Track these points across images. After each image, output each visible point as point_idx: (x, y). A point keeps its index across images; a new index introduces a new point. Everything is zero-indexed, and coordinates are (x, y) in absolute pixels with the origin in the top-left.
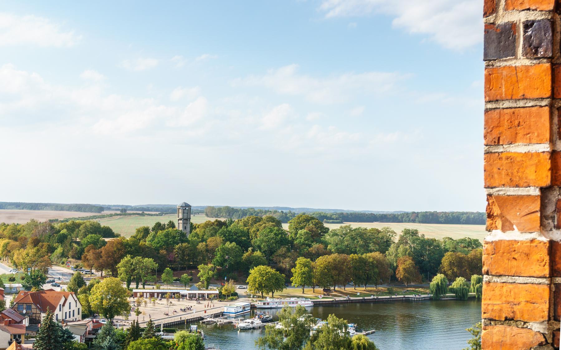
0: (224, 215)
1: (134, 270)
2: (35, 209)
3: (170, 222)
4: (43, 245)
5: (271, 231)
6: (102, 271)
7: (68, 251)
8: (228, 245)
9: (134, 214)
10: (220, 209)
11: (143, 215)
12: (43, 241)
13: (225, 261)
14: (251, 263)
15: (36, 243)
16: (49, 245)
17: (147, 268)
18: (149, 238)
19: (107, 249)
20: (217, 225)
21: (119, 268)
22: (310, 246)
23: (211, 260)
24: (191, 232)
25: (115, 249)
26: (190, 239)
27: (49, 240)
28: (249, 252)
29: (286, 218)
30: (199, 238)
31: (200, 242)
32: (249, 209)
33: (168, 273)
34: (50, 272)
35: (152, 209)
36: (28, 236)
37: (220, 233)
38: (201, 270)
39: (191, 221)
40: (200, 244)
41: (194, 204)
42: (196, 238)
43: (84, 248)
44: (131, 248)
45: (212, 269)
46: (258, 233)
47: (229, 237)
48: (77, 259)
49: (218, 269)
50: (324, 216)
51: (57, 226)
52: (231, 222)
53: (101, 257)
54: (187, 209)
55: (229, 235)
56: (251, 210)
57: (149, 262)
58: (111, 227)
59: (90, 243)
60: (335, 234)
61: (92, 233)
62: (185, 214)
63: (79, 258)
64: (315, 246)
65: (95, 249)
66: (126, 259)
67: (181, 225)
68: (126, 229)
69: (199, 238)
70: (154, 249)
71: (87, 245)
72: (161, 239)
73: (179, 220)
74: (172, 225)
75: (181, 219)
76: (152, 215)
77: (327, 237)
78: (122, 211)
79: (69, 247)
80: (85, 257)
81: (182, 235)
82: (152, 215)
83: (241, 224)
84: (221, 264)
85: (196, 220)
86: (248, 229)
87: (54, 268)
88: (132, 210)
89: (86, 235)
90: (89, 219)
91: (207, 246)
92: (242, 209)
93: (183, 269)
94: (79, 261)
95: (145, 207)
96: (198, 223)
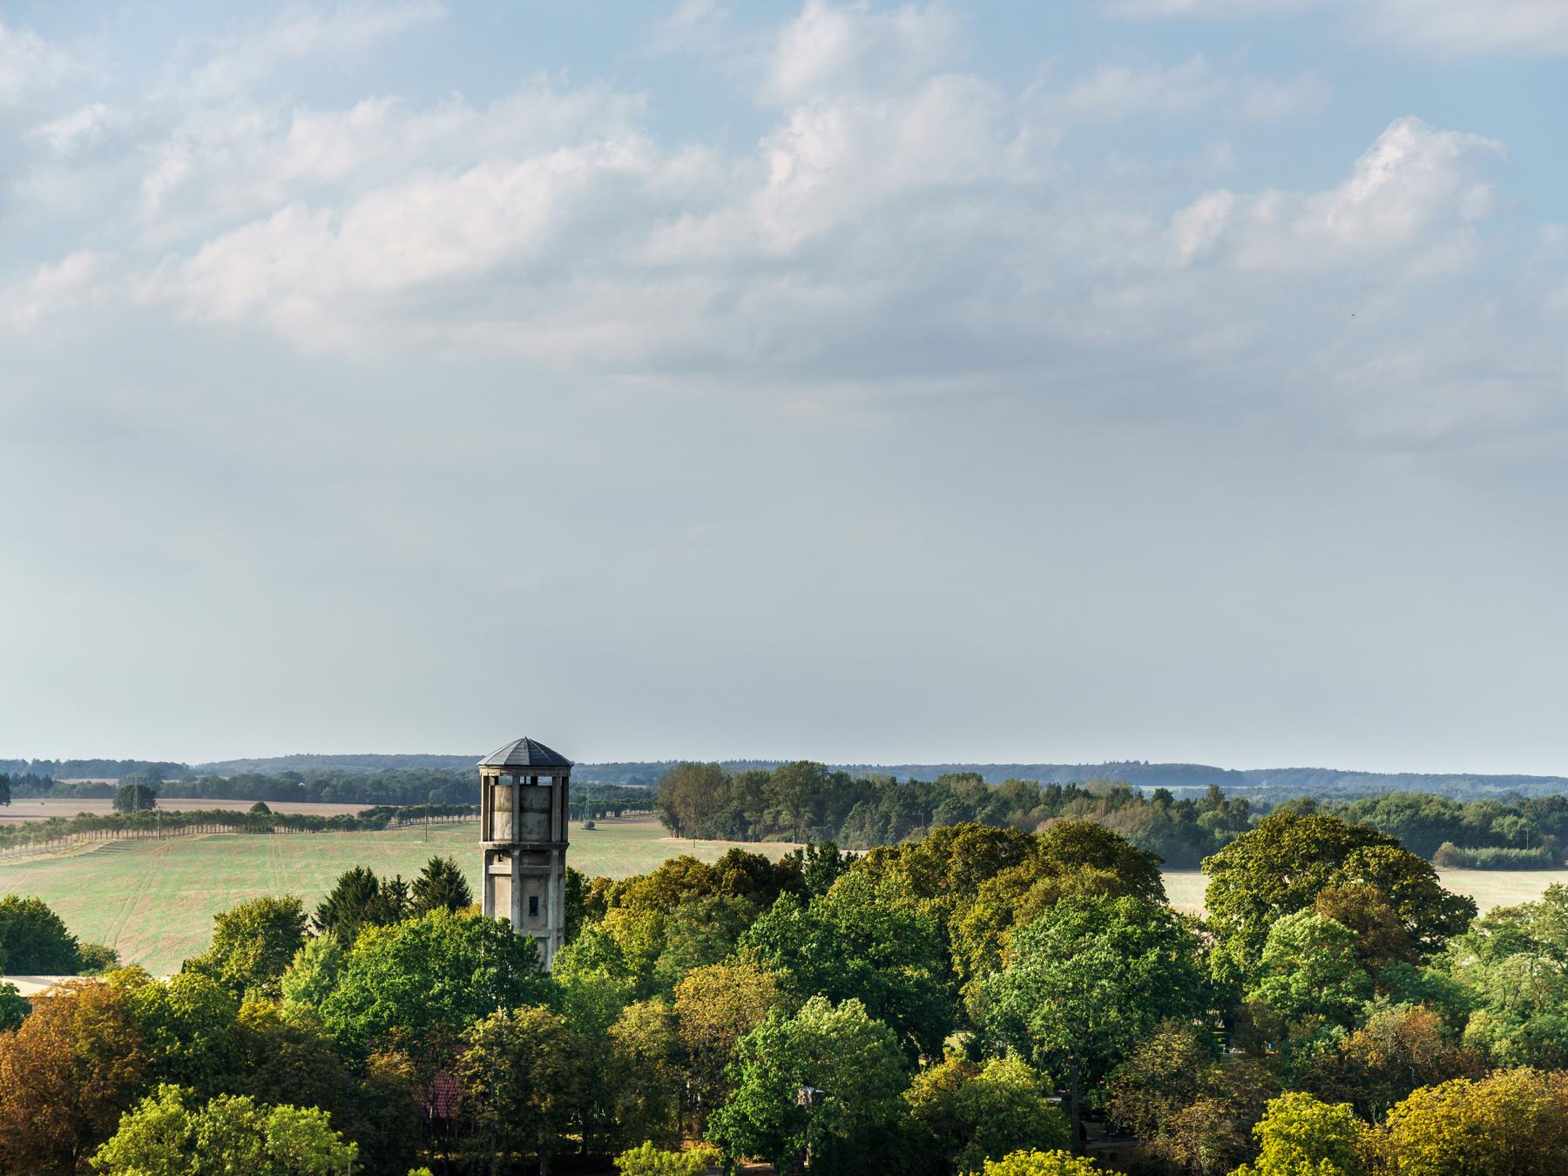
0: (786, 818)
3: (437, 868)
5: (1096, 922)
8: (817, 1015)
11: (259, 823)
13: (795, 1119)
18: (299, 975)
20: (739, 887)
22: (1349, 1018)
24: (569, 932)
25: (83, 1047)
26: (563, 980)
28: (951, 1063)
29: (1195, 822)
37: (762, 937)
39: (574, 861)
40: (633, 1012)
41: (588, 751)
44: (186, 1039)
46: (1007, 936)
52: (832, 866)
54: (543, 791)
56: (961, 788)
58: (55, 910)
60: (1512, 940)
62: (532, 819)
64: (1387, 1017)
66: (151, 1111)
67: (505, 889)
70: (335, 1046)
72: (380, 977)
74: (445, 886)
76: (316, 825)
77: (1463, 962)
81: (515, 953)
82: (316, 825)
83: (896, 876)
85: (605, 854)
86: (943, 913)
88: (193, 794)
91: (673, 1021)
95: (270, 772)
96: (618, 877)
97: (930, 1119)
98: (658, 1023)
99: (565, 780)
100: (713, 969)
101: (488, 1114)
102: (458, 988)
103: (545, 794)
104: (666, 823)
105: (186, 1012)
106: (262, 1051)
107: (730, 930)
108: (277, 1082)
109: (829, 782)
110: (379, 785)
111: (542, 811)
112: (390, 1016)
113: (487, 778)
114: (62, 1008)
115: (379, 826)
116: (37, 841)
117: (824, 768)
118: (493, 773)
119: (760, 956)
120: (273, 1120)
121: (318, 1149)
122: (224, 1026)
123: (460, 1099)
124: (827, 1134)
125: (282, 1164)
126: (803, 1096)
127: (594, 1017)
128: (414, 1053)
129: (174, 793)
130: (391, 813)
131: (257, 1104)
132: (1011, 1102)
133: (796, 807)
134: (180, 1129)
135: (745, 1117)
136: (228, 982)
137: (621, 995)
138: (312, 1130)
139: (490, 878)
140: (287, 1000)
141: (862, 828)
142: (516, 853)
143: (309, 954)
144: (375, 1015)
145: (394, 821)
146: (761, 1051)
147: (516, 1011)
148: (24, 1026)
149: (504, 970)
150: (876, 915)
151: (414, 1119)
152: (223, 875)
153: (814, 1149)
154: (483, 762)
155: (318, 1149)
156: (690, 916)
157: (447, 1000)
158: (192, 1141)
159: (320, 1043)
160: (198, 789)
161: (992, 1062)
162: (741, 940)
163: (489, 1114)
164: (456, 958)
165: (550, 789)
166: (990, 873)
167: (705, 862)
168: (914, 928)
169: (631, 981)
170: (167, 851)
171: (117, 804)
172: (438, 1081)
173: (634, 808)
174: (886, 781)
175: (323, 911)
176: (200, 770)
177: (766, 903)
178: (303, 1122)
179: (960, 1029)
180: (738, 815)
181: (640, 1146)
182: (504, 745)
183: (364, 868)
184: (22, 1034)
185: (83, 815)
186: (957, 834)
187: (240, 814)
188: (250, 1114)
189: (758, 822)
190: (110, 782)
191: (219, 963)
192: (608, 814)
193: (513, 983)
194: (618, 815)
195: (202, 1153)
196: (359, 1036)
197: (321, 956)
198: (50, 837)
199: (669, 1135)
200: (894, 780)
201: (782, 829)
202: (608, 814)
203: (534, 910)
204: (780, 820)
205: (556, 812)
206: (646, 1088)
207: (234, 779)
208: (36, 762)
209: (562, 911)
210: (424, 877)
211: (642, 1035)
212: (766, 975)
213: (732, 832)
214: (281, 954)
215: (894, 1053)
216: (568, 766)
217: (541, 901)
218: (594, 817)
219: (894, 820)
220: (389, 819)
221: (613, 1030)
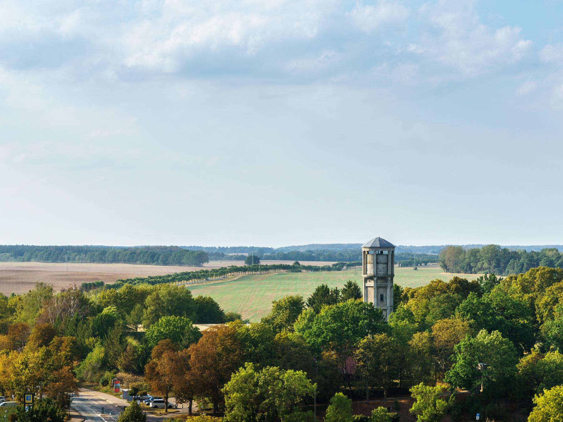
0: (486, 265)
1: (261, 397)
2: (55, 261)
3: (350, 284)
4: (61, 342)
6: (191, 400)
7: (117, 355)
8: (483, 336)
9: (275, 267)
10: (475, 253)
11: (296, 269)
12: (63, 333)
13: (477, 375)
14: (539, 380)
15: (47, 336)
16: (74, 342)
17: (291, 392)
18: (299, 324)
19: (201, 349)
20: (457, 290)
21: (227, 393)
23: (441, 372)
24: (394, 308)
25: (219, 349)
26: (392, 324)
27: (75, 331)
28: (534, 354)
30: (413, 321)
31: (415, 331)
32: (545, 250)
33: (340, 404)
34: (75, 402)
35: (320, 255)
36: (29, 321)
37: (464, 309)
38: (419, 397)
40: (417, 336)
41: (401, 240)
42: (406, 321)
43: (151, 348)
44: (256, 346)
45: (443, 395)
46: (555, 308)
47: (483, 319)
48: (135, 373)
49: (458, 396)
50: (87, 250)
51: (94, 297)
52: (493, 282)
53: (189, 369)
55: (483, 314)
56: (550, 254)
57: (293, 377)
58: (216, 300)
59: (165, 336)
61: (170, 313)
62: (381, 266)
63: (140, 372)
65: (174, 350)
66: (243, 372)
67: (372, 293)
68: (250, 304)
69: (413, 322)
70: (309, 348)
71: (158, 339)
72: (326, 324)
73: (366, 280)
74: (353, 291)
75: (371, 278)
76: (316, 269)
78: (249, 260)
79: (118, 347)
80: (153, 369)
81: (375, 315)
82: (316, 269)
83: (515, 286)
84: (468, 383)
85: (405, 278)
86: (533, 299)
87: (85, 394)
88: (274, 258)
89: (158, 317)
90: (173, 280)
91: (432, 339)
92: (528, 251)
93: (377, 395)
94: (141, 378)
95: (302, 250)
96: (414, 287)
97: (526, 375)
98: (426, 340)
99: (393, 252)
100: (446, 320)
101: (365, 373)
102: (354, 328)
103: (385, 257)
104: (442, 267)
105: (256, 337)
106: (283, 350)
107: (453, 306)
108: (289, 361)
109: (501, 252)
110: (341, 255)
111: (384, 264)
112: (330, 338)
113: (364, 252)
114: (212, 335)
115: (339, 269)
116: (216, 276)
117: (499, 247)
118: (367, 250)
119: (463, 316)
120: (286, 375)
121: (302, 386)
122: (269, 342)
123: (355, 367)
124: (488, 380)
125: (290, 391)
126: (480, 366)
127: (403, 337)
128: (338, 350)
129: (268, 258)
130: (344, 264)
131: (280, 369)
132: (556, 368)
133: (490, 261)
134: (253, 379)
135: (458, 374)
136: (276, 326)
137: (413, 330)
138: (300, 379)
139: (366, 288)
140: (295, 332)
141: (514, 268)
142: (375, 279)
143: (303, 315)
144: (324, 338)
145: (345, 267)
146: (463, 349)
147: (375, 336)
148: (199, 342)
149: (371, 321)
150: (506, 300)
151: (338, 375)
152: (282, 287)
153: (484, 385)
154: (363, 246)
155: (302, 386)
156: (437, 301)
157: (350, 332)
158: (257, 382)
159: (304, 348)
160: (276, 257)
161: (548, 354)
162: (456, 310)
163: (365, 373)
164: (353, 317)
165: (387, 255)
166: (550, 285)
167: (445, 281)
168: (521, 305)
169: (416, 325)
170: (262, 279)
171: (246, 263)
172: (347, 361)
173: (432, 262)
174: (522, 251)
175: (310, 300)
176: (278, 250)
177: (465, 296)
178: (297, 376)
179: (539, 342)
180: (469, 264)
181: (419, 384)
182: (371, 239)
183: (325, 285)
184: (199, 345)
185: (232, 266)
186: (538, 271)
187: (289, 266)
188: (278, 373)
189: (475, 267)
190: (245, 254)
191: (273, 319)
192: (423, 264)
193: (374, 326)
194: (426, 264)
195: (261, 387)
196: (318, 346)
197: (308, 316)
198: (221, 274)
199: (430, 380)
200: (525, 251)
201: (484, 269)
202: (423, 264)
203: (382, 299)
204: (484, 266)
205: (390, 264)
206: (422, 363)
207: (289, 253)
208: (219, 247)
209: (393, 299)
210: (345, 288)
211: (420, 344)
212: (465, 322)
213: (466, 270)
214: (295, 315)
215: (512, 351)
216: (394, 247)
217: (384, 296)
218: (417, 265)
219: (525, 265)
220: (343, 267)
221: (410, 343)
